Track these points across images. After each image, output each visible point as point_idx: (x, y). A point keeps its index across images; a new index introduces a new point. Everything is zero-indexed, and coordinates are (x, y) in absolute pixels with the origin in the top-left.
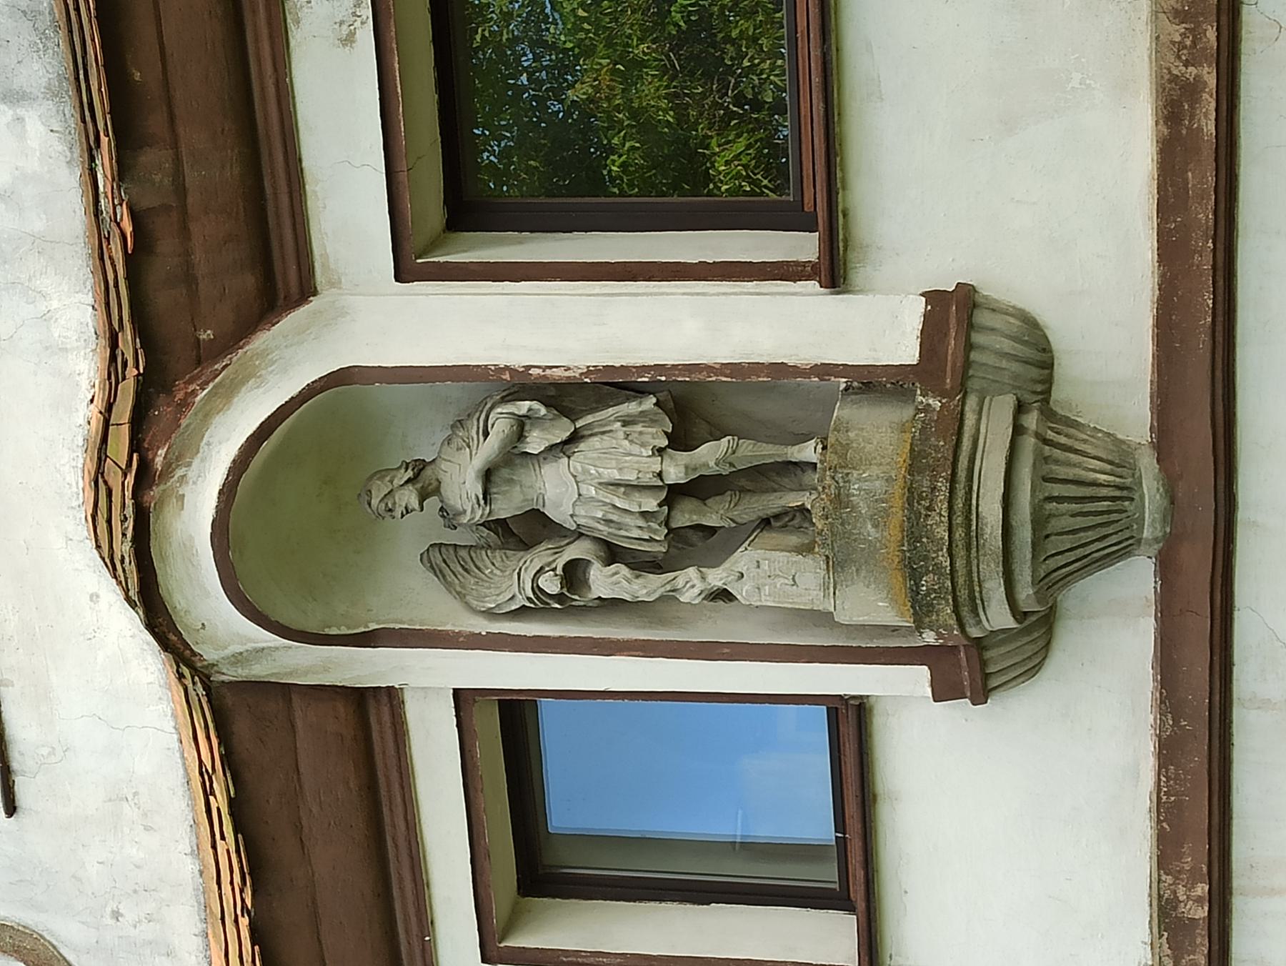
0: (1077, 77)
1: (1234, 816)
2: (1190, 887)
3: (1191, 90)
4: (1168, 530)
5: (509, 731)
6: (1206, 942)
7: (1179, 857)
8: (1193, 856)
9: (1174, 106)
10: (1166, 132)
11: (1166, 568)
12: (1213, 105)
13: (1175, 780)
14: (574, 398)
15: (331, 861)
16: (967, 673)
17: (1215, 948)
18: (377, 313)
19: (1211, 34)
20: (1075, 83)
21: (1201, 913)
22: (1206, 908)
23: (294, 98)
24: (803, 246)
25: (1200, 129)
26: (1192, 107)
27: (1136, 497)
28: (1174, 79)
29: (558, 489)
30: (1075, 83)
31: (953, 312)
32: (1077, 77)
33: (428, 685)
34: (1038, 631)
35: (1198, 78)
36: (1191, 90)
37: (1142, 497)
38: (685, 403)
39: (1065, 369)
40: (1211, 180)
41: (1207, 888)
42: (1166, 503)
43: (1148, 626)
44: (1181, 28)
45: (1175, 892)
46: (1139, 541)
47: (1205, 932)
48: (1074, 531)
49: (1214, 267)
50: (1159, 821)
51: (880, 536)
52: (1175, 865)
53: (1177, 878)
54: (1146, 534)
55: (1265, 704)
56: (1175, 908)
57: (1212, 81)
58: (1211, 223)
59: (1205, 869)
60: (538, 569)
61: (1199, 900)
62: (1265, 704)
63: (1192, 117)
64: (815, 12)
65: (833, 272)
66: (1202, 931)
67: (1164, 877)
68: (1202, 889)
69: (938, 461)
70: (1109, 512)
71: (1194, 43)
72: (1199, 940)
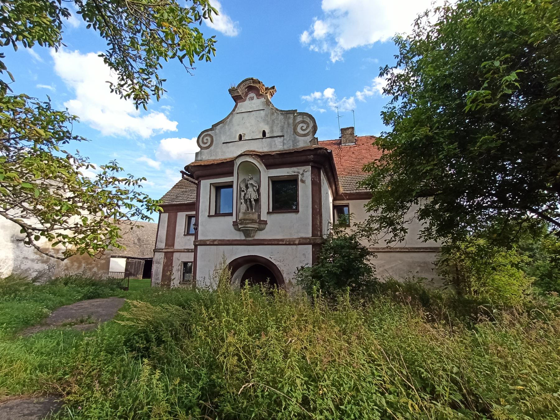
5: (230, 186)
9: (282, 240)
14: (258, 191)
15: (219, 170)
16: (235, 224)
18: (266, 174)
24: (271, 210)
29: (250, 189)
31: (265, 223)
33: (234, 179)
34: (239, 230)
38: (257, 201)
48: (247, 233)
51: (247, 217)
60: (244, 188)
65: (269, 213)
69: (253, 221)
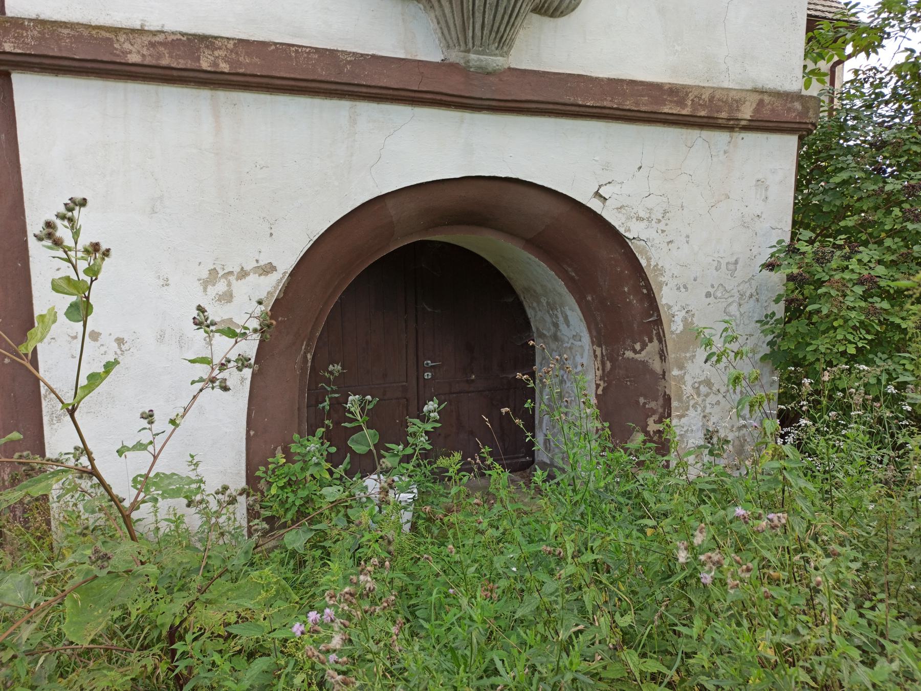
0: (678, 48)
1: (273, 97)
2: (225, 59)
3: (681, 103)
4: (472, 70)
6: (180, 66)
7: (248, 54)
8: (249, 64)
10: (666, 88)
11: (446, 66)
12: (675, 112)
13: (308, 58)
17: (175, 73)
19: (703, 113)
20: (677, 47)
21: (205, 65)
22: (209, 69)
23: (88, 26)
25: (665, 105)
26: (675, 102)
27: (497, 52)
28: (687, 94)
30: (677, 47)
32: (678, 48)
35: (686, 105)
36: (681, 103)
37: (495, 55)
39: (548, 22)
40: (643, 108)
41: (226, 70)
42: (490, 69)
43: (401, 55)
44: (707, 99)
45: (220, 48)
46: (468, 51)
47: (189, 66)
49: (604, 108)
50: (275, 44)
52: (240, 49)
53: (232, 51)
54: (473, 56)
55: (353, 121)
56: (207, 47)
57: (684, 112)
58: (625, 107)
59: (241, 71)
61: (215, 64)
62: (353, 121)
63: (671, 101)
64: (471, 3)
66: (190, 64)
67: (231, 42)
68: (224, 67)
70: (497, 32)
71: (700, 105)
72: (182, 61)
